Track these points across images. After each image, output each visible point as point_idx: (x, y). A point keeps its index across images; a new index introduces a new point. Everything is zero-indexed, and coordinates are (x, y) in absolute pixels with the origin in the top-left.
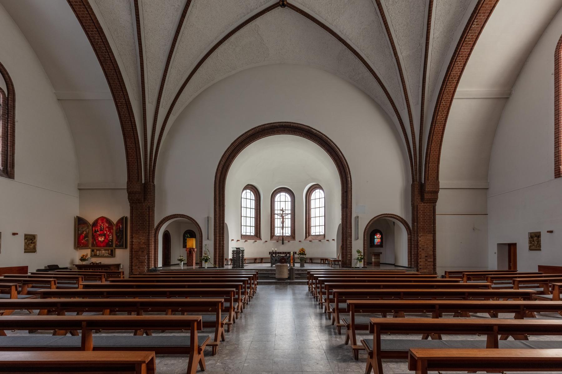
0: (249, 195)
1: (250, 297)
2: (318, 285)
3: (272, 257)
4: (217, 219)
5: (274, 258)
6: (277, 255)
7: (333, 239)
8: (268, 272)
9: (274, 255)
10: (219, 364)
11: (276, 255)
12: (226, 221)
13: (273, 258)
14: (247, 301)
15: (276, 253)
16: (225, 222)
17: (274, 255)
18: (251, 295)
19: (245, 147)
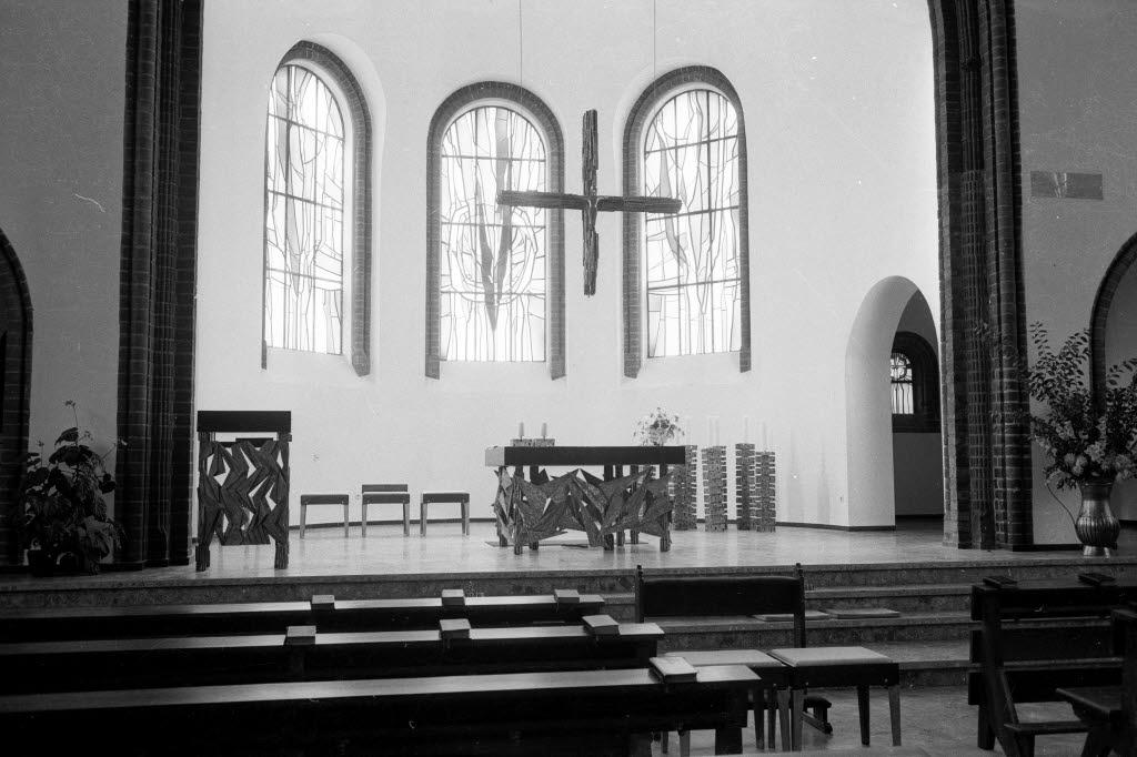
0: (316, 100)
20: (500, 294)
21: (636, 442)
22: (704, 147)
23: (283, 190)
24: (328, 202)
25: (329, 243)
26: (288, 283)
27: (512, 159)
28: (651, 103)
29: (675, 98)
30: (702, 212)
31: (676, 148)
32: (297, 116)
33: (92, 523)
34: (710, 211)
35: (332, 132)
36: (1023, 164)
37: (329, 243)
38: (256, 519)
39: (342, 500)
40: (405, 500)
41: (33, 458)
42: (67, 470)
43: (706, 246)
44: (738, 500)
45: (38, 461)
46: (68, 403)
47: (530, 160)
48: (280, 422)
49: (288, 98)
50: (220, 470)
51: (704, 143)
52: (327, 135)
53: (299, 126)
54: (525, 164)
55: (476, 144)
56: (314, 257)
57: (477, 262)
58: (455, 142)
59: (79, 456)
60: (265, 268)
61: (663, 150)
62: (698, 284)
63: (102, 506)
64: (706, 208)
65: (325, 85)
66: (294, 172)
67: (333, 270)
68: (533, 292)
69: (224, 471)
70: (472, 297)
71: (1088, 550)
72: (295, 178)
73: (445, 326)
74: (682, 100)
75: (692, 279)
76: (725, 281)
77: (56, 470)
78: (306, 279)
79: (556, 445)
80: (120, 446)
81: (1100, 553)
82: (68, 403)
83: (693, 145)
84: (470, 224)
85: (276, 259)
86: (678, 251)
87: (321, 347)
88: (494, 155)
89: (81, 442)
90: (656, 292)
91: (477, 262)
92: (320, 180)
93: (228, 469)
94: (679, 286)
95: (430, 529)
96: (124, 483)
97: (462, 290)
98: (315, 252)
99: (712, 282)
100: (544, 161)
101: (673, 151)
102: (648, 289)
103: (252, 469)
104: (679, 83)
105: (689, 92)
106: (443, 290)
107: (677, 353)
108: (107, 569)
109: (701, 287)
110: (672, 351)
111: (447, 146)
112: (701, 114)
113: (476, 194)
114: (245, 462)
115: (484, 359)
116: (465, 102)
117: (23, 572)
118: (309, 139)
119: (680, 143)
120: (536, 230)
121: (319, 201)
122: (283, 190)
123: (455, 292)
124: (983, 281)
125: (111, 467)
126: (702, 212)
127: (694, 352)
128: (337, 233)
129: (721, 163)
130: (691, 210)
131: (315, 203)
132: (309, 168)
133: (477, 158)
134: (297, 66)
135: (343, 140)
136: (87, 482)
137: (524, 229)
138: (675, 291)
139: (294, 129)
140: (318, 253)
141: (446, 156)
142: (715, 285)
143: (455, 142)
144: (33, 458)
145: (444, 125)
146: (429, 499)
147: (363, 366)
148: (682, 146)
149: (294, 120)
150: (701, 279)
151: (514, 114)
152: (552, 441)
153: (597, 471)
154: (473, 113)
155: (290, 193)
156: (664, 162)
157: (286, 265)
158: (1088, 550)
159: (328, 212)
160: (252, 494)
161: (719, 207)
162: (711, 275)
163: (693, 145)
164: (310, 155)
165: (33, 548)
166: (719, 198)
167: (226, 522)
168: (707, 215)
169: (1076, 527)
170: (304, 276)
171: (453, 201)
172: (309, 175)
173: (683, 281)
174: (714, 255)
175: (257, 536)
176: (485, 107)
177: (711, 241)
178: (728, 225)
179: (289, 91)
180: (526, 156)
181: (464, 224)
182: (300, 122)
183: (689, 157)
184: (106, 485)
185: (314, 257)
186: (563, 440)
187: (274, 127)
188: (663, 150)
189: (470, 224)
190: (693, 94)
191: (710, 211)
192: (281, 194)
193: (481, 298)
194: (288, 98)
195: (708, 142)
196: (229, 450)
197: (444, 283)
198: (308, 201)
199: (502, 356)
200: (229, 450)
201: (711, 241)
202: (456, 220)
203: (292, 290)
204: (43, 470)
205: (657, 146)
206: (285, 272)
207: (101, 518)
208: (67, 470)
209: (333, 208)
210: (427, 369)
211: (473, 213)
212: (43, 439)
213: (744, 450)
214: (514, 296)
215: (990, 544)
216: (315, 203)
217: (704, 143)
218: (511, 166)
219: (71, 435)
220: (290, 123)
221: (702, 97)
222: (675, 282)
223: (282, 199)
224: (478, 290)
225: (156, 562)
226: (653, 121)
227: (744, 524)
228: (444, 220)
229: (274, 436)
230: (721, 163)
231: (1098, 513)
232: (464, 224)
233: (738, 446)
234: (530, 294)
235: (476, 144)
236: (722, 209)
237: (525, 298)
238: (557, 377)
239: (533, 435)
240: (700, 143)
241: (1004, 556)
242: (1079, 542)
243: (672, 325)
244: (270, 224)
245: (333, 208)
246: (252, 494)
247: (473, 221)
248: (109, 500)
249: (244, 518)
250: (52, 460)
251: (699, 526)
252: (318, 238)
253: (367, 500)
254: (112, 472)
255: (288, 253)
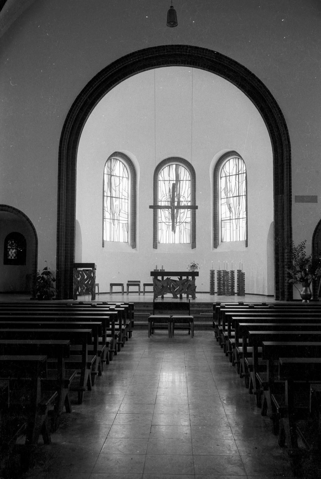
0: (119, 168)
1: (111, 352)
2: (250, 349)
3: (156, 281)
4: (63, 216)
5: (159, 282)
6: (165, 278)
7: (179, 18)
8: (147, 307)
9: (160, 278)
10: (65, 443)
11: (163, 278)
12: (78, 217)
13: (158, 283)
14: (115, 348)
15: (163, 273)
16: (76, 219)
17: (160, 278)
18: (121, 342)
19: (111, 87)
20: (176, 223)
21: (187, 270)
22: (237, 176)
23: (109, 195)
24: (123, 197)
25: (124, 209)
26: (111, 222)
27: (180, 180)
28: (223, 161)
29: (229, 160)
30: (237, 196)
31: (230, 176)
32: (113, 173)
33: (51, 289)
34: (239, 196)
35: (124, 176)
36: (292, 194)
37: (124, 209)
38: (87, 288)
39: (121, 285)
40: (139, 285)
41: (38, 274)
42: (45, 276)
43: (238, 207)
44: (237, 287)
45: (39, 274)
46: (46, 261)
47: (186, 180)
48: (92, 265)
49: (111, 169)
50: (79, 277)
51: (237, 174)
52: (123, 177)
53: (114, 176)
54: (184, 182)
55: (169, 176)
56: (119, 214)
57: (169, 213)
58: (163, 176)
59: (47, 273)
60: (103, 218)
61: (226, 176)
62: (235, 219)
63: (52, 284)
64: (238, 195)
65: (122, 163)
66: (112, 189)
67: (125, 217)
68: (187, 221)
69: (79, 277)
70: (168, 223)
71: (304, 301)
72: (113, 192)
73: (160, 233)
74: (231, 161)
75: (234, 218)
76: (243, 218)
77: (43, 276)
78: (117, 221)
79: (165, 271)
80: (57, 271)
81: (306, 302)
82: (46, 261)
83: (234, 175)
84: (168, 201)
85: (107, 215)
86: (230, 208)
87: (121, 240)
88: (175, 179)
89: (48, 270)
90: (224, 221)
91: (169, 213)
92: (121, 191)
93: (80, 276)
94: (230, 219)
95: (146, 294)
96: (58, 280)
97: (164, 221)
98: (120, 212)
99: (239, 219)
100: (190, 180)
101: (229, 177)
102: (222, 220)
103: (86, 277)
104: (229, 156)
105: (233, 158)
106: (159, 222)
107: (230, 241)
108: (54, 299)
109: (236, 220)
110: (228, 240)
111: (160, 177)
112: (236, 165)
113: (169, 192)
114: (84, 275)
115: (172, 243)
116: (165, 164)
117: (36, 299)
118: (117, 179)
119: (230, 174)
120: (188, 202)
121: (120, 197)
122: (109, 195)
123: (163, 222)
124: (283, 226)
125: (55, 276)
126: (237, 196)
127: (234, 241)
128: (126, 206)
129: (242, 181)
130: (234, 196)
131: (119, 198)
132: (117, 188)
133: (169, 180)
134: (113, 159)
135: (128, 178)
136: (49, 279)
137: (184, 202)
138: (229, 221)
139: (113, 177)
140: (120, 213)
141: (160, 180)
142: (240, 219)
143: (163, 176)
144: (38, 274)
145: (159, 171)
146: (145, 285)
147: (134, 245)
148: (231, 175)
149: (113, 174)
150: (236, 218)
151: (181, 166)
152: (164, 270)
153: (176, 278)
154: (168, 167)
155: (111, 196)
156: (226, 179)
157: (111, 217)
158: (304, 301)
159: (123, 200)
160: (86, 283)
161: (241, 195)
162: (239, 216)
163: (234, 175)
164: (118, 184)
165: (38, 294)
166: (241, 192)
167: (80, 289)
168: (238, 197)
169: (301, 295)
170: (116, 220)
171: (162, 194)
172: (117, 190)
173: (231, 218)
174: (240, 210)
175: (87, 293)
176: (172, 165)
177: (239, 206)
178: (243, 200)
179: (111, 166)
180: (185, 179)
181: (165, 201)
182: (115, 175)
183: (233, 178)
184: (54, 280)
185: (119, 214)
186: (167, 270)
187: (106, 177)
188: (226, 176)
189: (168, 201)
190: (234, 159)
191: (239, 196)
192: (109, 196)
193: (171, 224)
194: (111, 169)
195: (238, 174)
196: (81, 272)
197: (159, 220)
198: (117, 198)
199: (177, 242)
200: (81, 272)
201: (239, 206)
202: (163, 200)
203: (112, 224)
204: (40, 277)
205: (224, 175)
206: (110, 219)
207: (53, 288)
208: (45, 276)
209: (125, 199)
210: (153, 247)
211: (168, 198)
212: (40, 269)
213: (239, 271)
214: (181, 223)
215: (283, 300)
216: (119, 198)
217: (237, 174)
218: (180, 183)
219: (46, 269)
220: (111, 176)
221: (237, 160)
222: (229, 218)
223: (109, 198)
224: (170, 221)
225: (66, 298)
226: (223, 168)
227: (239, 294)
228: (159, 200)
229: (91, 269)
230: (242, 181)
231: (306, 290)
232: (165, 201)
233: (238, 270)
234: (186, 222)
235: (169, 176)
236: (242, 196)
237: (184, 224)
238: (194, 248)
239: (159, 268)
240: (236, 175)
241: (285, 302)
242: (302, 299)
243: (228, 231)
244: (105, 205)
245: (125, 199)
246: (86, 283)
247: (168, 200)
248: (54, 284)
249: (84, 288)
250: (42, 274)
251: (235, 295)
252: (120, 208)
253: (128, 285)
254: (55, 278)
255: (111, 214)
